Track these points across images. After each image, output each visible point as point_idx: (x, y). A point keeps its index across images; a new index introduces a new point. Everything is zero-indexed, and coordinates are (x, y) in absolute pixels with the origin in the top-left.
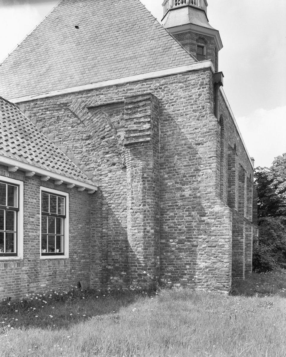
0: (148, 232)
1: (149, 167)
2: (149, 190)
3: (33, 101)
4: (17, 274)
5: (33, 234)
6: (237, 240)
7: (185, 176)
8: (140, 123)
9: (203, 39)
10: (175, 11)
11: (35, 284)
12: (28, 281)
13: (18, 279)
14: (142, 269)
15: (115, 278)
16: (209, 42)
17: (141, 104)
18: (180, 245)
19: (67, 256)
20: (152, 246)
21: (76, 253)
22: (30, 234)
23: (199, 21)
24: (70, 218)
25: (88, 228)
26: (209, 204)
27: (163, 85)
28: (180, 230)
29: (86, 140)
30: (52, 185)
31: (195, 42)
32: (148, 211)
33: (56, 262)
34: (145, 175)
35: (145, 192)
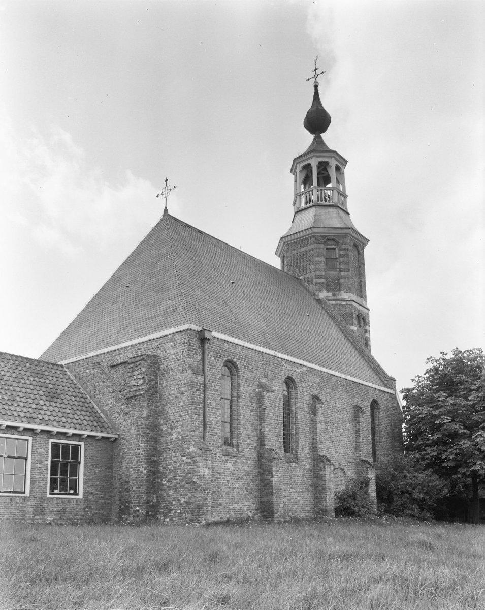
0: (141, 472)
1: (143, 416)
2: (143, 436)
3: (78, 361)
4: (22, 507)
5: (40, 477)
6: (268, 480)
7: (173, 422)
8: (137, 379)
9: (333, 240)
10: (302, 212)
11: (41, 517)
12: (34, 514)
13: (23, 511)
14: (136, 506)
15: (126, 517)
16: (341, 242)
17: (138, 363)
18: (169, 483)
19: (81, 496)
20: (145, 485)
21: (92, 494)
22: (37, 477)
23: (332, 219)
24: (85, 464)
25: (109, 472)
26: (187, 446)
27: (160, 344)
28: (169, 470)
29: (112, 393)
30: (63, 437)
31: (322, 246)
32: (142, 454)
33: (66, 501)
34: (139, 424)
35: (139, 438)
